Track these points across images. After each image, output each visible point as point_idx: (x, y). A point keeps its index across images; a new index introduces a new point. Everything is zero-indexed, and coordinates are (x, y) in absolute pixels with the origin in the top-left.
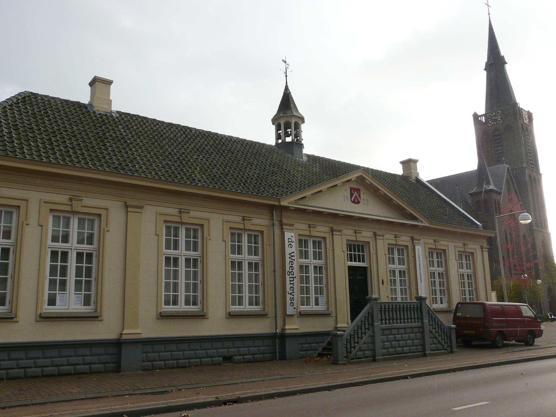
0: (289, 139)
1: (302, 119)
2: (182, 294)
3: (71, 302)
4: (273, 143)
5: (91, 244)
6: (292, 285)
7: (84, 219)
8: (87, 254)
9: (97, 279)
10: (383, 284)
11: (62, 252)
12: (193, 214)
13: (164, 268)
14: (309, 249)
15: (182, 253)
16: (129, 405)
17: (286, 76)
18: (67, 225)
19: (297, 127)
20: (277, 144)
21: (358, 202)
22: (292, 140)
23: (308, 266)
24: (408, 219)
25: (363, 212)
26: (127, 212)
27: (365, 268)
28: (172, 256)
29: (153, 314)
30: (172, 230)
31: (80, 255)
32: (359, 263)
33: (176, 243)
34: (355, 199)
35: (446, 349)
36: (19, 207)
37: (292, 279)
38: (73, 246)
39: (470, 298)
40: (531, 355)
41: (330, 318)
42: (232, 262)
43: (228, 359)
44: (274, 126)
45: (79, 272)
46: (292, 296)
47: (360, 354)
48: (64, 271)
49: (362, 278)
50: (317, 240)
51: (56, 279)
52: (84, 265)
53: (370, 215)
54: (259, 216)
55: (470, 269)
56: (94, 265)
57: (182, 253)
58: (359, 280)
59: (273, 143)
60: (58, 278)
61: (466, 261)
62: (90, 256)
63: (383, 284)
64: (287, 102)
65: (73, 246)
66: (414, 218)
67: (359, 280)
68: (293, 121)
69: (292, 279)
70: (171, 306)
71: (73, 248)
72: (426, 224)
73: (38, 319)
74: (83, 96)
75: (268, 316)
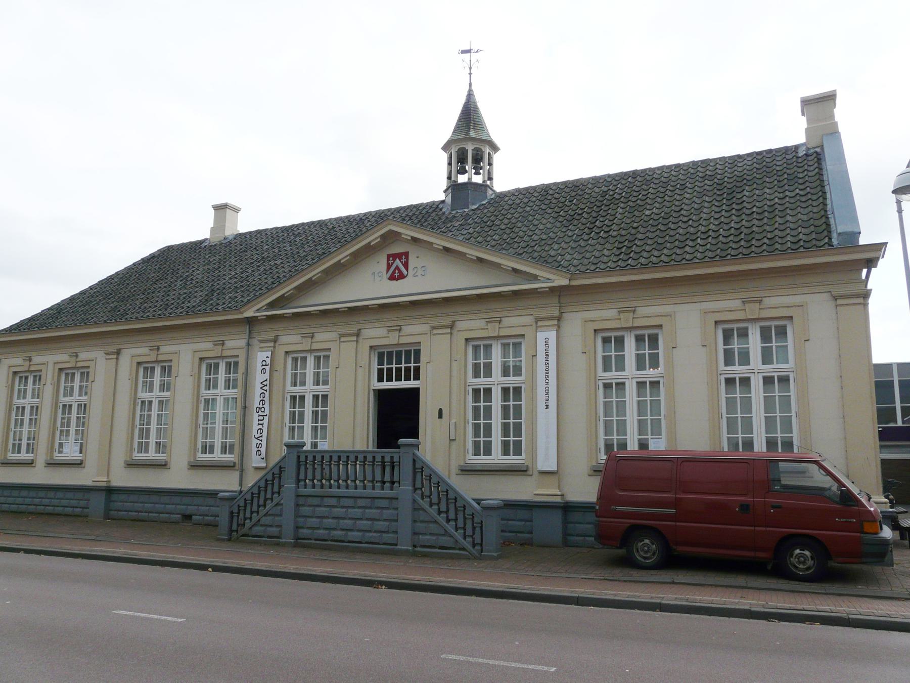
2: (497, 438)
3: (70, 452)
6: (260, 427)
7: (509, 344)
11: (514, 388)
15: (309, 389)
16: (122, 550)
17: (470, 74)
18: (488, 355)
20: (454, 188)
21: (402, 277)
23: (304, 396)
25: (420, 291)
26: (837, 306)
28: (482, 387)
29: (184, 464)
30: (732, 332)
31: (505, 391)
33: (620, 360)
34: (394, 272)
36: (791, 317)
37: (261, 418)
38: (497, 380)
40: (820, 607)
41: (529, 478)
43: (187, 517)
47: (258, 530)
50: (646, 332)
54: (170, 342)
57: (630, 372)
58: (397, 415)
62: (325, 397)
64: (469, 117)
65: (497, 380)
67: (397, 415)
68: (487, 150)
69: (261, 418)
71: (756, 371)
75: (530, 472)
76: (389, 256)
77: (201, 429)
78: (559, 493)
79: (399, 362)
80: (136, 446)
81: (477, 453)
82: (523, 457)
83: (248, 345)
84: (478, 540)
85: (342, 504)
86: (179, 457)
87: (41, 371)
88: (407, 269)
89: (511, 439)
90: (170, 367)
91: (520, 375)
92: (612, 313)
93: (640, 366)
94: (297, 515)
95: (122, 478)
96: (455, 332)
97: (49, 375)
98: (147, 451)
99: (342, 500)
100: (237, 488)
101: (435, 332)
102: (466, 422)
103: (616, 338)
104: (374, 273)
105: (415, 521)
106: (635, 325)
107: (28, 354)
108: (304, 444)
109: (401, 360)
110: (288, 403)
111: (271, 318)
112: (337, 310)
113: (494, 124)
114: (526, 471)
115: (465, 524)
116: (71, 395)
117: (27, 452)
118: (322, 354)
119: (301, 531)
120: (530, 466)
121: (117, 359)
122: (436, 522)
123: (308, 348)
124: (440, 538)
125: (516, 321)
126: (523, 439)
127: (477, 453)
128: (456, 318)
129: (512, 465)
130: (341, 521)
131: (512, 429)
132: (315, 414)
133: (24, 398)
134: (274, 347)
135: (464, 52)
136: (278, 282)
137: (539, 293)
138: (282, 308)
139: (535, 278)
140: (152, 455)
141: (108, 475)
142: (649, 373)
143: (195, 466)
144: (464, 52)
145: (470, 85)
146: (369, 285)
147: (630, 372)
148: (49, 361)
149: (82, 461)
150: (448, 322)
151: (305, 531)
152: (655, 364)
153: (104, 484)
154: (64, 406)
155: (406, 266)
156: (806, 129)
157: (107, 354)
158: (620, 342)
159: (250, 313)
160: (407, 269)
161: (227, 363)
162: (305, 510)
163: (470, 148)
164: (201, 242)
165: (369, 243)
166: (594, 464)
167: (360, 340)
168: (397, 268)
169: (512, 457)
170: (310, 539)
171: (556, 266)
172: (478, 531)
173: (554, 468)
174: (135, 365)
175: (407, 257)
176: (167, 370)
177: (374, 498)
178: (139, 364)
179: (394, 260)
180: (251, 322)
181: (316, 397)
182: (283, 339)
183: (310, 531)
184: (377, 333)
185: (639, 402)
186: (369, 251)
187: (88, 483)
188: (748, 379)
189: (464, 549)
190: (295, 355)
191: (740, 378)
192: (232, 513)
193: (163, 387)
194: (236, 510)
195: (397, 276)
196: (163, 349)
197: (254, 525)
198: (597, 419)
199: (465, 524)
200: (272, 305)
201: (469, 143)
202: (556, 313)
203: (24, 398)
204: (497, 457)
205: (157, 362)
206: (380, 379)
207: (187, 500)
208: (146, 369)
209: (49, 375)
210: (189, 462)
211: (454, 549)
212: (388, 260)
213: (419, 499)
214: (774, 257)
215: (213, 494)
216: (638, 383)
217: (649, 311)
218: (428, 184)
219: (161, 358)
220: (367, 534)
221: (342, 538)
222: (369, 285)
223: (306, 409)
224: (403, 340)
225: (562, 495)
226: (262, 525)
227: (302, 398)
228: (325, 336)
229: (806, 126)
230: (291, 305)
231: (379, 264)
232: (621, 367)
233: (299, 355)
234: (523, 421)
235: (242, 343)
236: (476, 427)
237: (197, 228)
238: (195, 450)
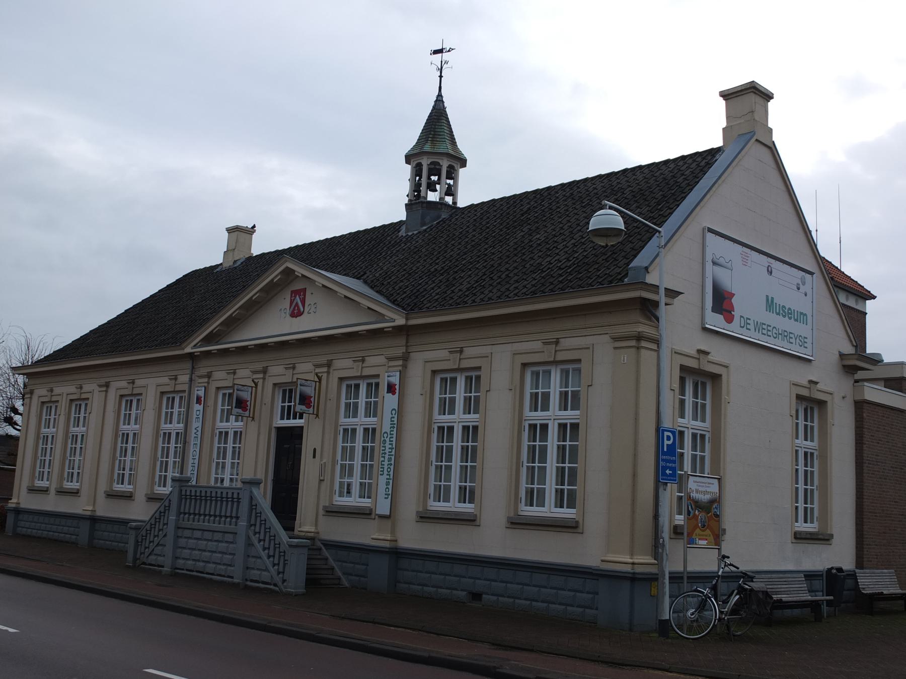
1: (463, 162)
2: (551, 486)
9: (428, 463)
10: (315, 450)
11: (572, 424)
14: (459, 464)
17: (441, 77)
19: (452, 174)
20: (416, 203)
21: (300, 314)
22: (440, 199)
23: (355, 429)
27: (16, 439)
32: (288, 421)
34: (294, 309)
35: (275, 585)
39: (216, 479)
43: (476, 596)
44: (409, 167)
49: (831, 598)
50: (353, 382)
55: (812, 441)
61: (806, 420)
62: (575, 427)
63: (315, 450)
64: (438, 121)
68: (445, 164)
72: (400, 321)
76: (292, 292)
77: (525, 469)
80: (431, 490)
83: (191, 380)
86: (494, 507)
87: (479, 368)
89: (566, 487)
90: (478, 378)
95: (412, 537)
97: (150, 399)
98: (541, 504)
99: (226, 535)
100: (682, 569)
102: (334, 462)
103: (451, 378)
107: (79, 382)
108: (188, 480)
110: (525, 435)
114: (474, 520)
116: (452, 412)
117: (806, 522)
118: (570, 367)
121: (106, 391)
123: (456, 367)
128: (213, 369)
129: (807, 533)
132: (561, 449)
133: (355, 416)
134: (208, 383)
135: (436, 52)
136: (205, 321)
138: (217, 343)
140: (454, 505)
141: (94, 505)
143: (517, 523)
144: (436, 52)
146: (275, 324)
148: (65, 390)
149: (78, 490)
153: (387, 544)
154: (346, 430)
156: (724, 129)
157: (615, 339)
159: (188, 350)
161: (467, 378)
162: (182, 542)
163: (425, 162)
164: (217, 266)
165: (273, 280)
166: (512, 515)
170: (192, 571)
173: (387, 512)
174: (429, 374)
176: (474, 381)
178: (525, 365)
180: (191, 356)
181: (562, 427)
182: (338, 364)
186: (272, 291)
187: (79, 511)
190: (370, 381)
193: (472, 405)
195: (296, 313)
196: (469, 352)
197: (150, 554)
198: (519, 464)
200: (208, 340)
201: (436, 150)
202: (400, 351)
203: (355, 416)
204: (549, 510)
205: (460, 370)
208: (443, 380)
209: (150, 399)
210: (509, 518)
211: (270, 584)
213: (251, 534)
215: (124, 522)
219: (465, 364)
222: (275, 324)
223: (549, 443)
227: (544, 427)
229: (724, 125)
231: (284, 302)
233: (448, 376)
237: (212, 253)
238: (426, 495)
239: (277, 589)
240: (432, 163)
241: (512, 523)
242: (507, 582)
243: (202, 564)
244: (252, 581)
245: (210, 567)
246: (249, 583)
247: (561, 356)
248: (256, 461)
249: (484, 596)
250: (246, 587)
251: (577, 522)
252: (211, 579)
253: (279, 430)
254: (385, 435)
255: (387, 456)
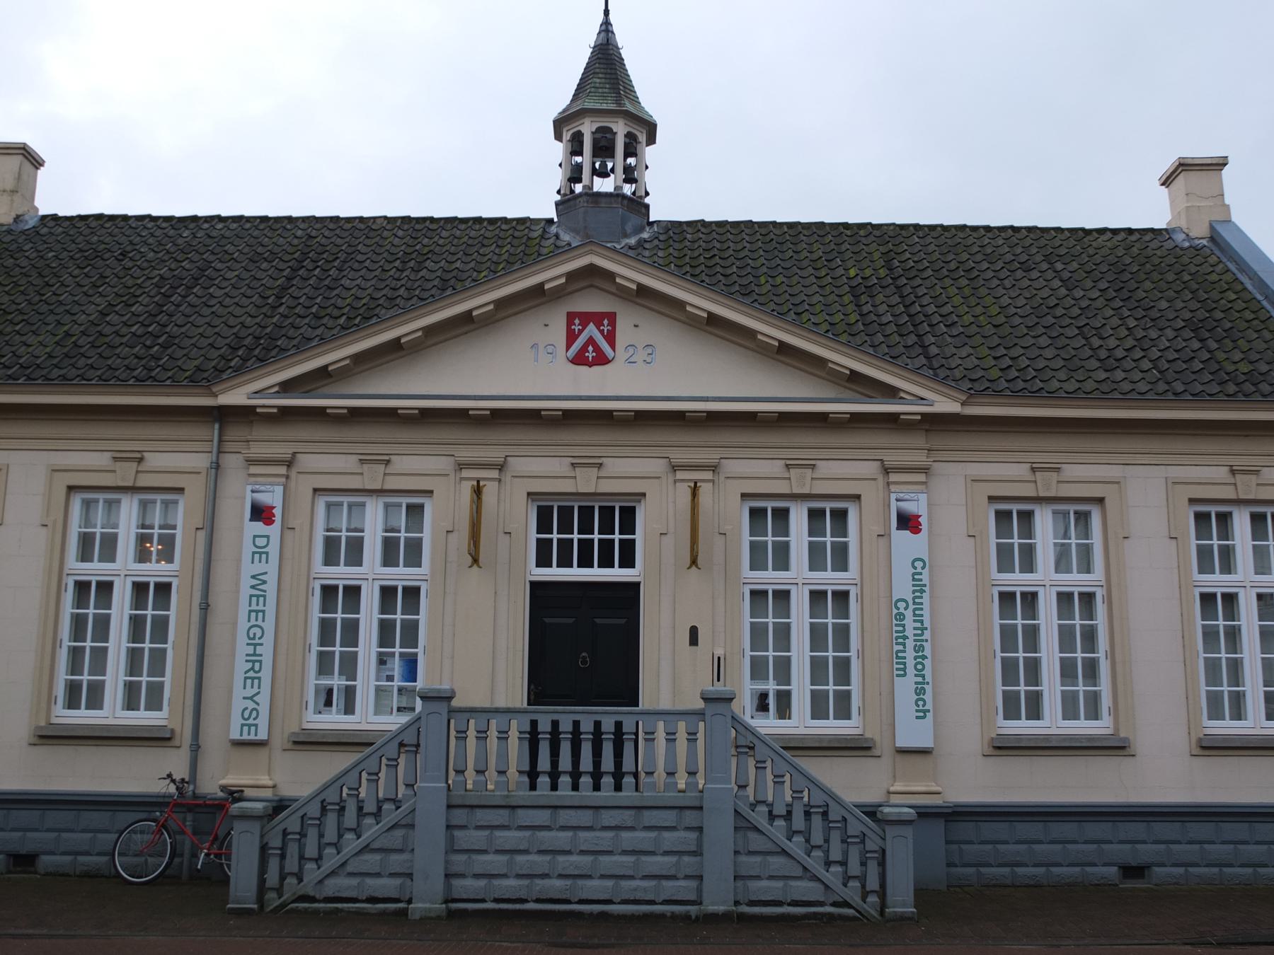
0: (604, 185)
4: (543, 206)
5: (845, 569)
8: (1081, 594)
11: (1224, 595)
12: (1071, 471)
13: (1199, 623)
18: (1225, 532)
20: (566, 203)
21: (602, 360)
24: (869, 398)
27: (635, 586)
28: (94, 579)
30: (1013, 517)
31: (1064, 599)
33: (1227, 556)
34: (584, 349)
42: (1001, 594)
43: (1133, 871)
45: (817, 637)
46: (251, 705)
48: (351, 630)
51: (334, 652)
52: (1019, 622)
53: (706, 399)
56: (1101, 620)
58: (585, 644)
59: (543, 206)
60: (831, 654)
64: (606, 65)
66: (891, 393)
67: (585, 644)
68: (620, 129)
70: (1228, 722)
73: (990, 751)
74: (1149, 209)
76: (571, 317)
78: (270, 783)
79: (586, 528)
81: (72, 703)
82: (164, 713)
83: (217, 466)
84: (873, 884)
85: (562, 822)
88: (612, 345)
91: (113, 560)
92: (103, 460)
93: (816, 562)
94: (451, 849)
95: (972, 781)
96: (507, 478)
98: (1238, 714)
101: (254, 470)
103: (774, 510)
104: (534, 346)
105: (736, 853)
106: (387, 487)
109: (600, 524)
110: (69, 596)
111: (286, 415)
112: (463, 413)
113: (650, 93)
115: (846, 853)
119: (456, 882)
120: (178, 730)
122: (784, 852)
123: (130, 484)
124: (793, 883)
125: (842, 469)
126: (167, 679)
127: (72, 703)
129: (1090, 738)
130: (561, 858)
131: (833, 671)
137: (328, 415)
138: (307, 394)
139: (891, 393)
142: (829, 579)
145: (606, 12)
146: (525, 366)
147: (800, 576)
150: (283, 451)
151: (469, 882)
152: (841, 562)
155: (611, 339)
158: (782, 516)
159: (235, 396)
160: (612, 345)
163: (588, 128)
167: (293, 474)
168: (591, 341)
169: (831, 722)
171: (937, 371)
172: (873, 869)
174: (63, 491)
175: (613, 323)
177: (556, 807)
179: (585, 326)
183: (482, 883)
184: (548, 468)
185: (813, 627)
188: (787, 593)
189: (846, 904)
191: (775, 592)
192: (264, 848)
194: (276, 842)
196: (155, 460)
198: (56, 644)
199: (846, 853)
200: (287, 387)
201: (606, 111)
204: (1053, 723)
206: (543, 561)
207: (1136, 829)
212: (570, 322)
214: (35, 389)
216: (812, 593)
217: (1083, 470)
218: (521, 180)
220: (624, 883)
221: (394, 895)
223: (114, 612)
224: (606, 487)
225: (274, 787)
226: (351, 874)
228: (418, 463)
230: (326, 390)
231: (549, 329)
232: (782, 562)
234: (420, 650)
235: (201, 461)
236: (76, 654)
238: (51, 700)
239: (851, 912)
240: (599, 130)
241: (1204, 748)
242: (25, 830)
243: (558, 883)
244: (752, 903)
245: (595, 888)
246: (745, 909)
247: (144, 481)
248: (481, 648)
249: (45, 859)
250: (742, 917)
251: (172, 731)
252: (603, 915)
253: (536, 587)
254: (902, 605)
255: (910, 644)
